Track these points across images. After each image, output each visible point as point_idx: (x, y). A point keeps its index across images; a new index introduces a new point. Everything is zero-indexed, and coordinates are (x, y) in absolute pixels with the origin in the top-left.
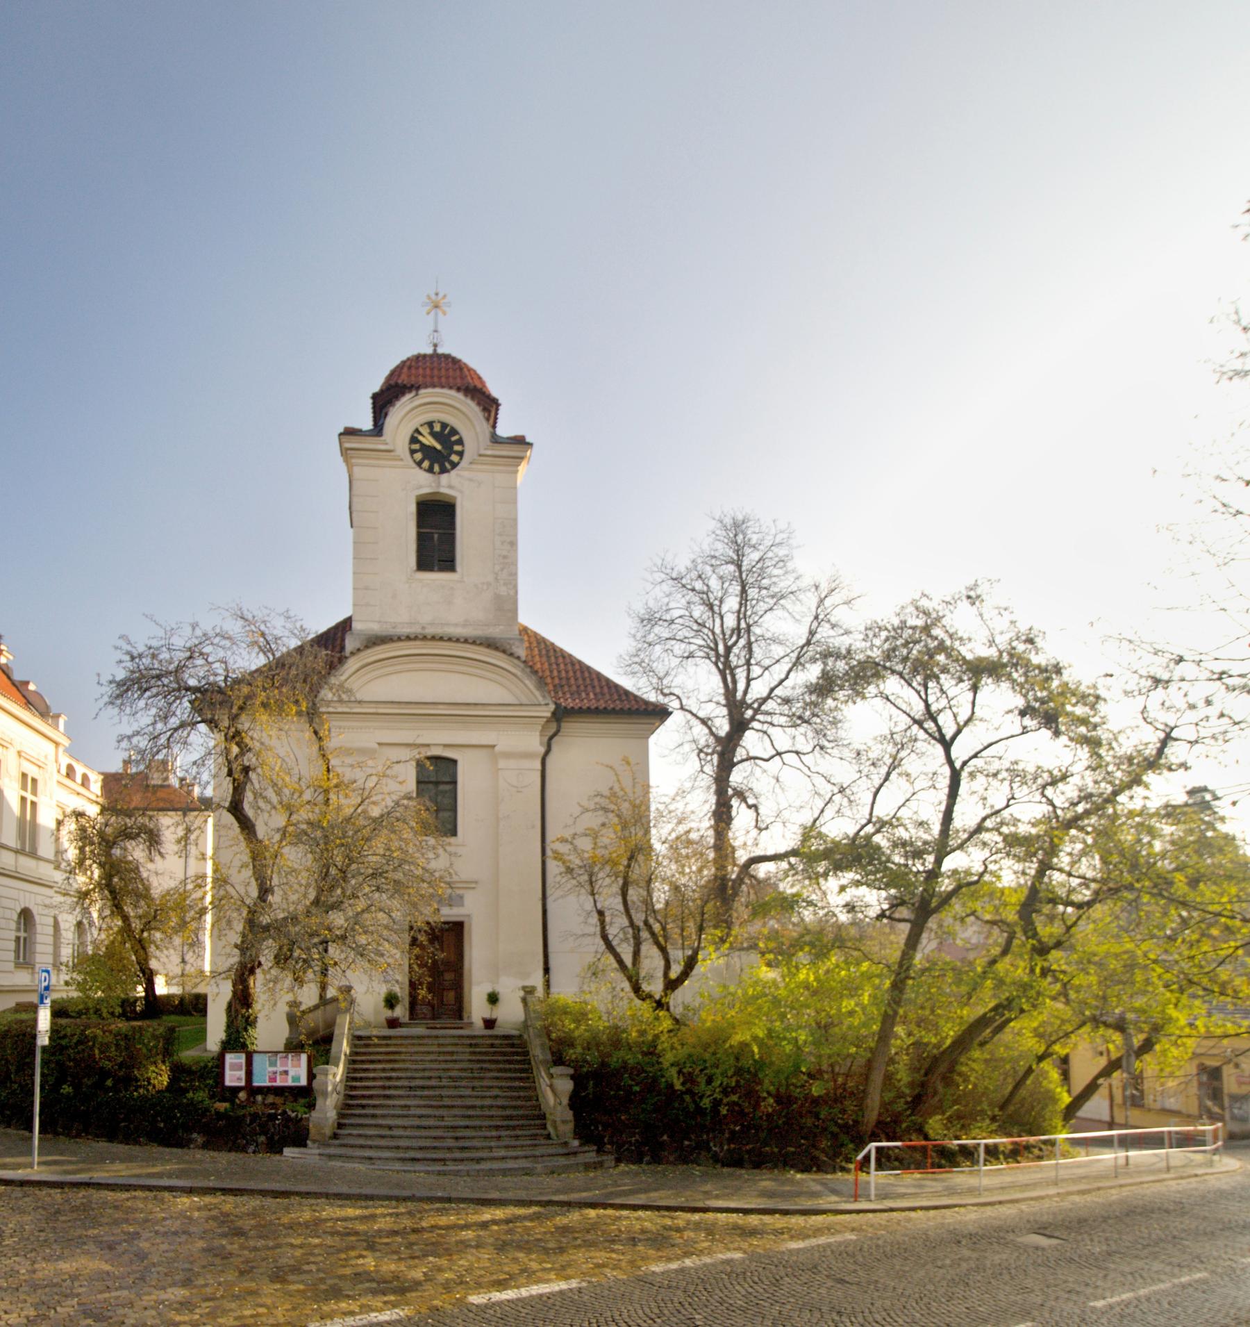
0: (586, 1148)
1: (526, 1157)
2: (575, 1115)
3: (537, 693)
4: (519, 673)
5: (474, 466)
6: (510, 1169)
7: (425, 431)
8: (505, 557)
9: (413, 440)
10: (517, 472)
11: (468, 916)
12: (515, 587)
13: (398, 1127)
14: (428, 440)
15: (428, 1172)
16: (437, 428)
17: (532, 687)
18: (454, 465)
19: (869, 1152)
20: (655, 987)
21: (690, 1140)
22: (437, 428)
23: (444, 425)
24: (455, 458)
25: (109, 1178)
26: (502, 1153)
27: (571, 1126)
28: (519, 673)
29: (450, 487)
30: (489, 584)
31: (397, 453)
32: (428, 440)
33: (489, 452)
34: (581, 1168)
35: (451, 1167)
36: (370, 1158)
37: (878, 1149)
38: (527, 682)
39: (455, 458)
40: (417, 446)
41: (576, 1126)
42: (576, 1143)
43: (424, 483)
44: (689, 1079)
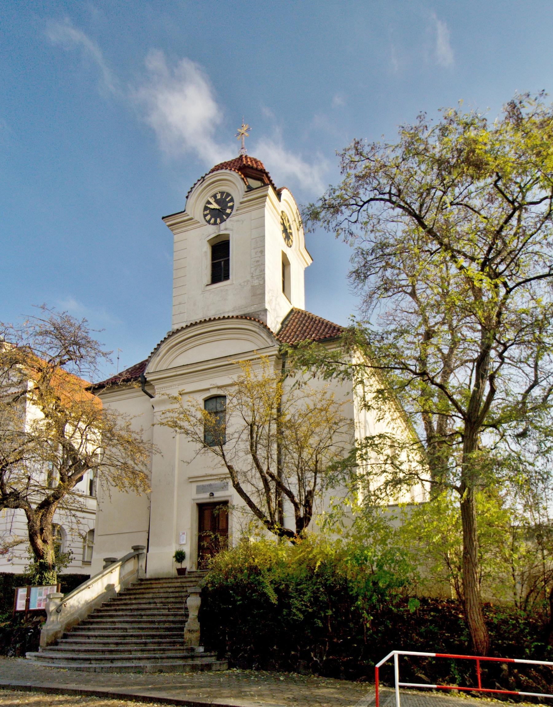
0: (208, 654)
1: (148, 659)
2: (201, 626)
3: (269, 340)
4: (257, 330)
5: (239, 212)
6: (125, 667)
7: (212, 201)
8: (258, 261)
9: (206, 208)
10: (264, 206)
11: (231, 496)
12: (264, 279)
13: (92, 636)
14: (215, 206)
15: (70, 669)
16: (219, 196)
17: (265, 337)
18: (228, 215)
19: (392, 659)
20: (291, 524)
21: (296, 650)
22: (219, 196)
23: (222, 193)
24: (228, 211)
25: (347, 684)
26: (139, 655)
27: (197, 635)
28: (257, 330)
29: (226, 229)
30: (248, 281)
31: (196, 219)
32: (215, 206)
33: (245, 199)
34: (188, 669)
35: (94, 665)
36: (52, 658)
37: (400, 656)
38: (262, 335)
39: (228, 211)
40: (208, 212)
41: (201, 637)
42: (201, 649)
43: (211, 231)
44: (282, 594)
